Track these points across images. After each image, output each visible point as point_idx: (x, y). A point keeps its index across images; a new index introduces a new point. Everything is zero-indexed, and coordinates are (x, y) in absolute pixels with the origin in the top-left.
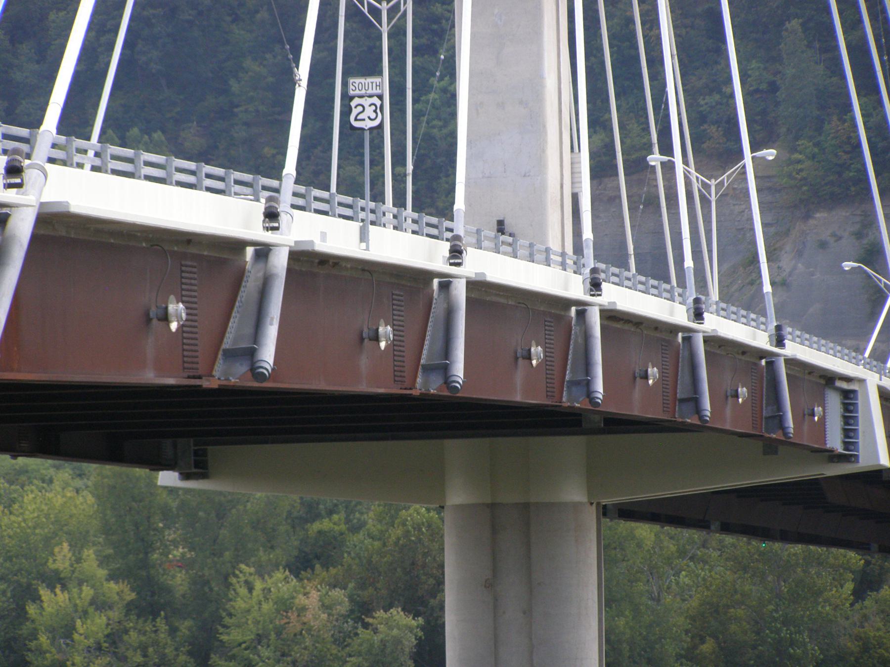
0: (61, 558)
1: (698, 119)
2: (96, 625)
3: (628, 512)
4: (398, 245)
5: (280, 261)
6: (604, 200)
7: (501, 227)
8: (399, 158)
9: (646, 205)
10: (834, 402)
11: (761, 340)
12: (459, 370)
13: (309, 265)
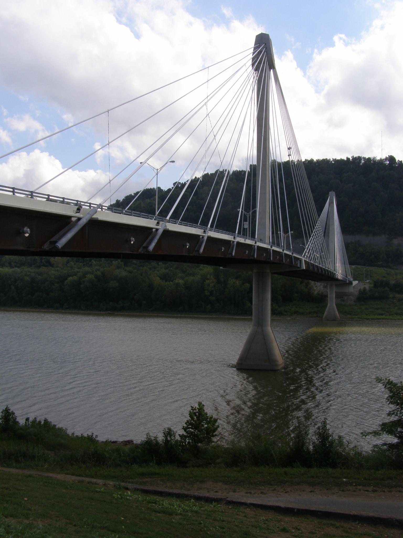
0: (208, 277)
1: (284, 228)
2: (212, 285)
3: (275, 273)
4: (249, 242)
5: (235, 243)
6: (273, 237)
7: (261, 240)
8: (249, 231)
9: (278, 237)
10: (299, 261)
11: (290, 254)
12: (256, 256)
13: (238, 243)
